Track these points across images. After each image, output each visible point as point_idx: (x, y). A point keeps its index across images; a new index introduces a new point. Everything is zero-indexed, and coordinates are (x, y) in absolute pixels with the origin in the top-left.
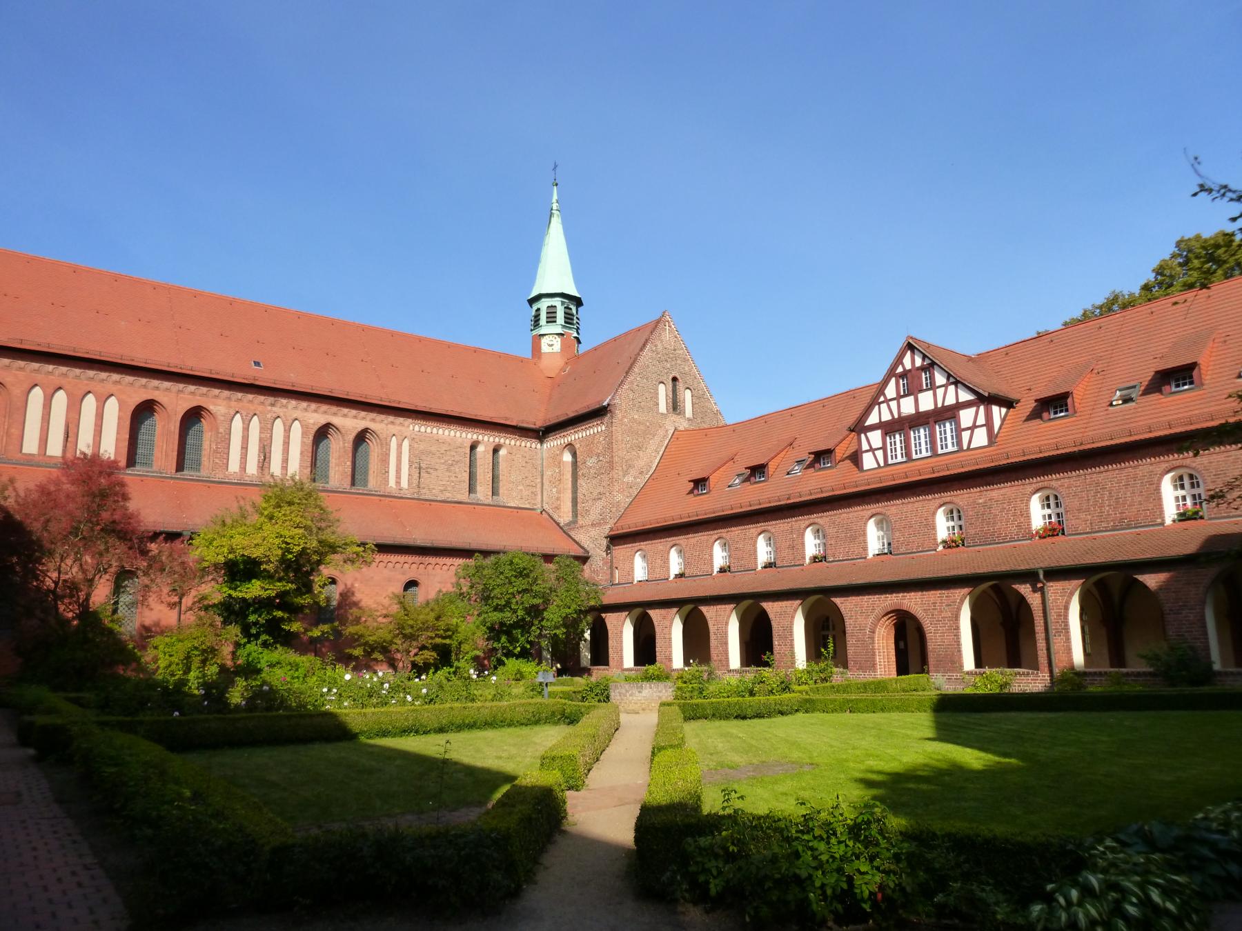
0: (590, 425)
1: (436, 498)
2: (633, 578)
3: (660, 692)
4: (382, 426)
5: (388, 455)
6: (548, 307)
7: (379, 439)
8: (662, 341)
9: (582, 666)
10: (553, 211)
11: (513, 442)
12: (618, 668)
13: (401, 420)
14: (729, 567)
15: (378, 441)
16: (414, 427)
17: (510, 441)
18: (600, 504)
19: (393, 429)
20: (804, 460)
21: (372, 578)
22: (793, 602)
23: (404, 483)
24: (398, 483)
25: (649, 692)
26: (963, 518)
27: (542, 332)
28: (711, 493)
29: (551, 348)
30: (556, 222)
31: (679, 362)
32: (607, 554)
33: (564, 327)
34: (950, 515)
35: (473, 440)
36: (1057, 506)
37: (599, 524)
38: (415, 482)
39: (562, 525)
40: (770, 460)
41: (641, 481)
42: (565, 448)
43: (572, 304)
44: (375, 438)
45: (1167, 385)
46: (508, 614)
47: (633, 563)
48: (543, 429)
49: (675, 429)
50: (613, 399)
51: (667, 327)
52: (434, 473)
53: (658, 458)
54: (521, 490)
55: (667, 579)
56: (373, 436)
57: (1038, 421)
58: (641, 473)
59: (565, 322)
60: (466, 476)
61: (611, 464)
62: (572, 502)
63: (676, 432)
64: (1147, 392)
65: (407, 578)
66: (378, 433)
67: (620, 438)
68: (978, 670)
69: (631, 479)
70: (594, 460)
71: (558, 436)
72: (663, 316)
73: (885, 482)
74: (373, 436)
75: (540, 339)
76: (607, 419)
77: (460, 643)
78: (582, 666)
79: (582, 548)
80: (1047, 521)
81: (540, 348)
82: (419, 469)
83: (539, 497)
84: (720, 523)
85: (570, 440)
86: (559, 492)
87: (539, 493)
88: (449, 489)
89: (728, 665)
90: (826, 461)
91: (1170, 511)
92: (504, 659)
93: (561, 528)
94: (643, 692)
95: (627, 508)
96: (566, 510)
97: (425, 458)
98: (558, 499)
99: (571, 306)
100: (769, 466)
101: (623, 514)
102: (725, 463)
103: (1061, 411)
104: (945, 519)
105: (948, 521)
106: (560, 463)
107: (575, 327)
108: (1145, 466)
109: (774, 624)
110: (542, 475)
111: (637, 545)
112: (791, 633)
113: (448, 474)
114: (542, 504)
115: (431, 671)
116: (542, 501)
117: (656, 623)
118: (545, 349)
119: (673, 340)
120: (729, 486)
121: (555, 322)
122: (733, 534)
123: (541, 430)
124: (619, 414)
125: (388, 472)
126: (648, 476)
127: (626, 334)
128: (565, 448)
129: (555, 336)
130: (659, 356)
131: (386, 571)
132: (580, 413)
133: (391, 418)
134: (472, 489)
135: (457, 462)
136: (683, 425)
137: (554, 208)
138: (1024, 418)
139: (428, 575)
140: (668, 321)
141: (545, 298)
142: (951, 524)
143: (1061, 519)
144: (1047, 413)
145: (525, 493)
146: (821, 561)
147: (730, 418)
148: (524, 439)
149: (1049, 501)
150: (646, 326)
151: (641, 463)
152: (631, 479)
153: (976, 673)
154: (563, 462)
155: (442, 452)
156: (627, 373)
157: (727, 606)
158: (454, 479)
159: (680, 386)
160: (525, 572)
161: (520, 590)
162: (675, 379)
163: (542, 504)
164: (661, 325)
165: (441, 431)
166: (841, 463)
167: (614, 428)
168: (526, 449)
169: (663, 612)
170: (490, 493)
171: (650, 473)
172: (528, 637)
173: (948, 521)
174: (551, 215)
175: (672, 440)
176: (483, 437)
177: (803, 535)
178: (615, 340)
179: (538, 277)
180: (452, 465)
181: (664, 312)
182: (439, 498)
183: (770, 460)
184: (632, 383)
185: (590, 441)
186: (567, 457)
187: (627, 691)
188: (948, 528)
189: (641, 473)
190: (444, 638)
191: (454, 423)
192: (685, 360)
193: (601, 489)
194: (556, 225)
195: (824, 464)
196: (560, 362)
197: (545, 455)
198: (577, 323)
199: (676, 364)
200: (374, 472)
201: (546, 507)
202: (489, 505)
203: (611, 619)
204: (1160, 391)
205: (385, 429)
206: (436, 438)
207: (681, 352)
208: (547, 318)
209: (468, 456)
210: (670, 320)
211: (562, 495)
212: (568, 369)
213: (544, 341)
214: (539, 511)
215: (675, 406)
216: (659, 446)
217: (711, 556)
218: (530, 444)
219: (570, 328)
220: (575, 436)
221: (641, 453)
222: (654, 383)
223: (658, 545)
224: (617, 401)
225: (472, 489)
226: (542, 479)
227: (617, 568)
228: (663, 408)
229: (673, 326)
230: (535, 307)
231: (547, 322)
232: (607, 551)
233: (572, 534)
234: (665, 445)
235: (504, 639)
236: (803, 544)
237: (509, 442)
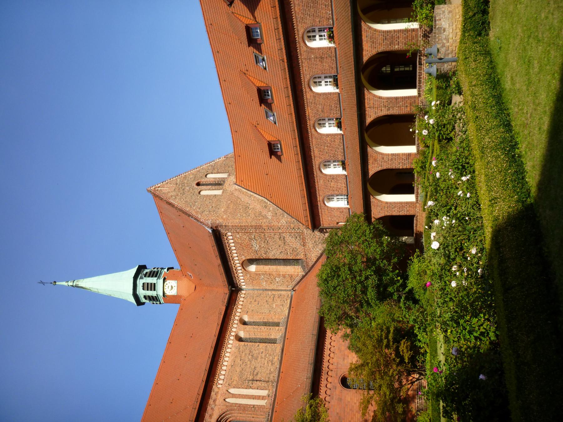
0: (227, 246)
1: (278, 370)
2: (345, 208)
3: (444, 12)
4: (216, 409)
5: (240, 405)
6: (143, 289)
7: (226, 412)
8: (169, 192)
9: (413, 242)
10: (74, 285)
11: (239, 310)
12: (416, 207)
13: (213, 394)
14: (337, 119)
15: (228, 413)
16: (219, 384)
17: (238, 312)
18: (289, 239)
19: (220, 400)
20: (255, 56)
21: (338, 413)
22: (363, 29)
23: (264, 393)
24: (263, 398)
25: (444, 21)
26: (319, 76)
27: (161, 294)
28: (280, 140)
29: (174, 288)
30: (83, 283)
31: (186, 182)
32: (327, 232)
33: (159, 278)
34: (321, 125)
35: (235, 339)
36: (314, 31)
37: (304, 239)
38: (264, 384)
39: (304, 274)
40: (255, 85)
41: (272, 207)
42: (245, 270)
43: (143, 272)
44: (226, 415)
45: (267, 100)
46: (370, 282)
47: (334, 208)
48: (230, 287)
49: (235, 184)
50: (207, 225)
51: (159, 189)
52: (258, 369)
53: (256, 195)
54: (276, 305)
55: (346, 176)
56: (224, 417)
57: (282, 157)
58: (266, 207)
59: (156, 276)
60: (262, 345)
61: (258, 227)
62: (287, 265)
63: (238, 184)
64: (260, 50)
65: (339, 386)
66: (221, 412)
67: (237, 221)
68: (417, 87)
69: (270, 214)
70: (254, 243)
71: (236, 275)
72: (151, 191)
73: (286, 76)
74: (224, 417)
75: (167, 296)
76: (223, 231)
77: (393, 320)
78: (413, 242)
79: (322, 255)
80: (329, 83)
81: (174, 296)
82: (252, 382)
83: (283, 293)
84: (303, 126)
85: (239, 265)
86: (279, 275)
87: (279, 292)
88: (271, 358)
89: (415, 97)
90: (276, 147)
91: (334, 130)
92: (407, 289)
93: (306, 274)
94: (444, 27)
95: (292, 217)
96: (293, 270)
97: (245, 375)
98: (284, 276)
99: (145, 272)
100: (270, 140)
101: (296, 219)
102: (258, 131)
103: (268, 92)
104: (314, 42)
105: (315, 40)
106: (257, 274)
107: (160, 270)
108: (302, 56)
109: (381, 49)
110: (266, 290)
111: (320, 204)
112: (390, 32)
113: (259, 359)
114: (288, 290)
115: (419, 344)
116: (285, 290)
117: (380, 168)
118: (173, 292)
119: (169, 185)
120: (275, 123)
121: (155, 284)
122: (311, 115)
123: (231, 289)
124: (219, 221)
125: (254, 405)
126: (269, 202)
127: (164, 223)
128: (245, 270)
129: (165, 284)
130: (179, 194)
131: (332, 403)
132: (218, 254)
133: (211, 401)
134: (273, 341)
135: (250, 351)
136: (233, 179)
137: (72, 285)
138: (280, 162)
139: (337, 369)
140: (155, 188)
141: (136, 292)
142: (327, 124)
143: (322, 29)
144: (268, 100)
145: (279, 302)
146: (332, 32)
147: (229, 149)
148: (237, 302)
149: (311, 36)
150: (159, 208)
151: (258, 207)
152: (270, 214)
153: (419, 88)
154: (255, 272)
155: (241, 362)
156: (189, 216)
157: (366, 97)
158: (263, 355)
159: (203, 180)
160: (334, 269)
161: (349, 272)
162: (198, 184)
163: (288, 290)
164: (157, 193)
165: (225, 363)
166: (257, 19)
167: (230, 224)
168: (245, 301)
169: (370, 161)
170: (277, 328)
171: (266, 201)
172: (389, 270)
173: (315, 40)
174: (77, 286)
175: (243, 186)
176: (233, 332)
177: (312, 49)
178: (176, 250)
179: (121, 297)
180: (252, 356)
181: (148, 191)
182: (278, 366)
183: (255, 85)
184: (197, 212)
185: (240, 246)
186: (253, 268)
187: (443, 46)
188: (330, 126)
189: (266, 207)
190: (389, 332)
191: (220, 353)
192: (185, 177)
193: (277, 237)
194: (85, 283)
195: (278, 149)
196: (185, 282)
197: (250, 287)
198: (157, 269)
199: (187, 183)
200: (253, 417)
201: (290, 288)
202: (286, 328)
203: (377, 213)
204: (260, 44)
205: (219, 407)
206: (230, 367)
207: (179, 180)
208: (151, 290)
209: (246, 343)
210: (154, 187)
211: (281, 273)
212: (190, 274)
213: (169, 292)
214: (293, 293)
215: (218, 184)
216: (246, 195)
217: (328, 135)
218: (242, 298)
219: (161, 273)
220: (236, 261)
221: (250, 207)
222: (199, 197)
223: (320, 184)
224: (210, 223)
225: (273, 341)
226: (269, 290)
227: (338, 223)
228: (219, 192)
229: (159, 185)
230: (143, 300)
231: (154, 290)
232: (325, 233)
233: (311, 264)
234: (246, 191)
235: (390, 289)
236: (319, 49)
237: (238, 313)
